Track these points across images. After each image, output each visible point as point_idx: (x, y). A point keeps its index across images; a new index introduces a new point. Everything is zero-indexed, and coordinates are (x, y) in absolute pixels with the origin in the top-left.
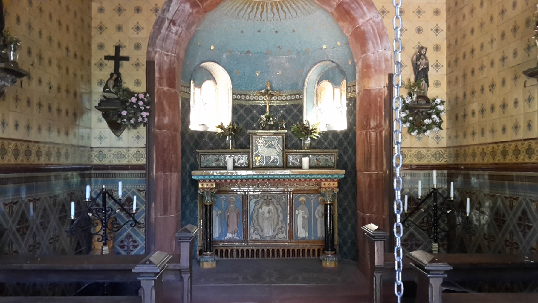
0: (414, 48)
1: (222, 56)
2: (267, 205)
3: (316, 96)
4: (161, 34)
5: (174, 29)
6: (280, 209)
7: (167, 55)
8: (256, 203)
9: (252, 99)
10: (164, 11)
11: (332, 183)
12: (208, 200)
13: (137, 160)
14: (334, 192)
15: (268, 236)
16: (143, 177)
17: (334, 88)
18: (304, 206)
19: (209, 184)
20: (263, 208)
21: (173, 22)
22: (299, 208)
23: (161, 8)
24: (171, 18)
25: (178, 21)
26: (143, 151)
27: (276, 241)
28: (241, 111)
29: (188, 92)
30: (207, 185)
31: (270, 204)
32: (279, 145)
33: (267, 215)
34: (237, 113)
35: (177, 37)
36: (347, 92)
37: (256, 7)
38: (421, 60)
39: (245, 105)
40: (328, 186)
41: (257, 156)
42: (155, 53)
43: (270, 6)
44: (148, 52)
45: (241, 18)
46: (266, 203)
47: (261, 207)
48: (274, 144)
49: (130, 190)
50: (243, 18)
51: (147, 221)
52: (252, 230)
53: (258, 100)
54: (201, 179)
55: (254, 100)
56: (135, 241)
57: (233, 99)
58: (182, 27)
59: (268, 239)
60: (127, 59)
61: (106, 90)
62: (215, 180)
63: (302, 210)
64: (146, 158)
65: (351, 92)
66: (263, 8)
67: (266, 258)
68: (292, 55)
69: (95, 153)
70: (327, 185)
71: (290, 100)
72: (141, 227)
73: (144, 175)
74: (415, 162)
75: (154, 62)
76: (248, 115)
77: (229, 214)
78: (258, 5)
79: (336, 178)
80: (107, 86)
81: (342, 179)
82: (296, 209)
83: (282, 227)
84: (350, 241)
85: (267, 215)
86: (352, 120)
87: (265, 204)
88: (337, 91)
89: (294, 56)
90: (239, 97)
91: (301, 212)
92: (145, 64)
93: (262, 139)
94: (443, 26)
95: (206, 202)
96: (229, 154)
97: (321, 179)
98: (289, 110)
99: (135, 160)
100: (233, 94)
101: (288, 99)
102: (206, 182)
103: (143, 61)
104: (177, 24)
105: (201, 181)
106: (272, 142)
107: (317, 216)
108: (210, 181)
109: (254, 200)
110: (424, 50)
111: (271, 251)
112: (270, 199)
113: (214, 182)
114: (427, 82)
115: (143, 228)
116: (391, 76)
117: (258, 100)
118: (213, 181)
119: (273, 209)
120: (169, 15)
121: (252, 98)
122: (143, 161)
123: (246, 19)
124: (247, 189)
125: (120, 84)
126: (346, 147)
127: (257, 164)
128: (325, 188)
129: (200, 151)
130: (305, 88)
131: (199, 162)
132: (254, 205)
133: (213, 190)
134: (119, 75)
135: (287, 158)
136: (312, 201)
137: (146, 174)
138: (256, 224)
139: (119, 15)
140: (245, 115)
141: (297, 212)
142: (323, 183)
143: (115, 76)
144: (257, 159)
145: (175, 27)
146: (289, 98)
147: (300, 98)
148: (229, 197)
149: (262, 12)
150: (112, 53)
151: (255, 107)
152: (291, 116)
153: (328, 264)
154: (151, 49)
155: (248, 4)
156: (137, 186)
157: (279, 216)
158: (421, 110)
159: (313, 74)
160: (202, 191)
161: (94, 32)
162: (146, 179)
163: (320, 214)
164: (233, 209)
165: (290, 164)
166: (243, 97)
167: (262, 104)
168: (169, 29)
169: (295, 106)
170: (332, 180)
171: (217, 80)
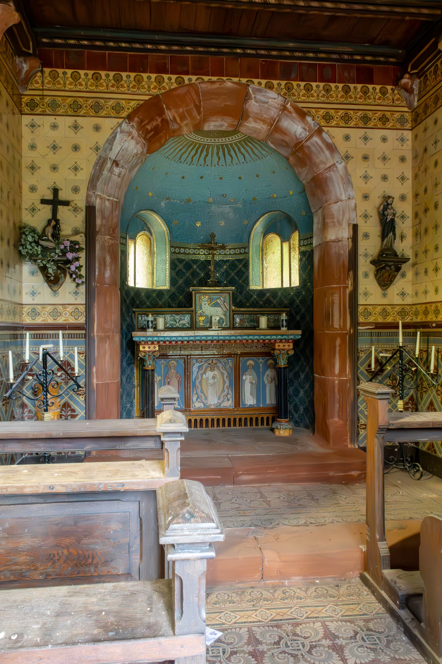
0: (379, 197)
1: (160, 204)
2: (212, 370)
3: (263, 251)
4: (103, 176)
5: (117, 170)
6: (226, 374)
7: (109, 200)
8: (199, 368)
9: (192, 253)
10: (105, 150)
11: (287, 344)
12: (149, 365)
13: (75, 319)
14: (288, 354)
15: (212, 404)
16: (82, 338)
17: (282, 242)
18: (252, 370)
19: (152, 347)
20: (207, 374)
21: (116, 163)
22: (247, 373)
23: (102, 146)
24: (114, 158)
25: (122, 162)
26: (82, 309)
27: (221, 410)
28: (180, 266)
29: (124, 243)
30: (149, 348)
31: (215, 369)
32: (225, 303)
33: (211, 381)
34: (175, 269)
35: (119, 179)
36: (300, 246)
37: (200, 150)
38: (388, 210)
39: (184, 260)
40: (283, 348)
41: (201, 315)
42: (96, 198)
43: (215, 149)
44: (88, 196)
45: (182, 163)
46: (210, 368)
47: (205, 373)
48: (219, 302)
49: (68, 353)
50: (185, 162)
51: (87, 388)
52: (195, 398)
53: (199, 254)
54: (143, 341)
55: (194, 254)
56: (73, 411)
57: (171, 251)
58: (126, 169)
59: (212, 407)
60: (66, 203)
61: (44, 238)
62: (158, 342)
63: (250, 376)
64: (86, 317)
65: (304, 245)
66: (207, 152)
67: (210, 428)
68: (237, 204)
69: (26, 309)
70: (281, 347)
71: (234, 254)
72: (80, 395)
73: (83, 335)
74: (380, 320)
75: (95, 207)
76: (187, 270)
77: (169, 380)
78: (204, 148)
79: (291, 339)
80: (45, 234)
81: (299, 340)
82: (244, 374)
83: (228, 394)
84: (302, 407)
85: (211, 381)
86: (306, 276)
87: (209, 369)
88: (286, 246)
89: (240, 206)
90: (177, 250)
91: (248, 377)
92: (84, 209)
93: (207, 297)
94: (409, 174)
95: (148, 367)
96: (170, 314)
97: (275, 341)
98: (233, 265)
99: (73, 319)
100: (171, 247)
101: (231, 253)
102: (148, 344)
103: (82, 205)
104: (120, 166)
105: (143, 343)
106: (218, 300)
107: (266, 382)
108: (153, 343)
109: (197, 365)
110: (391, 199)
111: (215, 420)
112: (215, 364)
113: (157, 344)
114: (394, 234)
115: (83, 395)
116: (355, 228)
117: (199, 254)
118: (156, 343)
119: (218, 375)
120: (113, 155)
121: (191, 251)
122: (82, 320)
123: (189, 163)
124: (179, 352)
125: (58, 232)
126: (298, 306)
127: (201, 324)
128: (279, 350)
129: (137, 310)
130: (251, 241)
131: (135, 323)
132: (198, 369)
133: (156, 353)
134: (57, 221)
135: (233, 318)
136: (261, 365)
137: (85, 335)
138: (199, 391)
139: (54, 153)
140: (184, 271)
141: (244, 377)
142: (277, 345)
143: (53, 223)
144: (202, 319)
145: (118, 168)
146: (232, 252)
147: (245, 252)
148: (168, 362)
149: (207, 156)
150: (49, 196)
151: (195, 262)
152: (235, 271)
153: (281, 432)
154: (91, 193)
155: (193, 146)
156: (81, 348)
157: (224, 382)
158: (390, 264)
159: (259, 227)
160: (143, 354)
161: (26, 173)
162: (86, 341)
163: (269, 379)
164: (174, 375)
165: (237, 325)
166: (182, 250)
167: (202, 258)
168: (111, 170)
169: (240, 261)
170: (287, 341)
171: (152, 231)
